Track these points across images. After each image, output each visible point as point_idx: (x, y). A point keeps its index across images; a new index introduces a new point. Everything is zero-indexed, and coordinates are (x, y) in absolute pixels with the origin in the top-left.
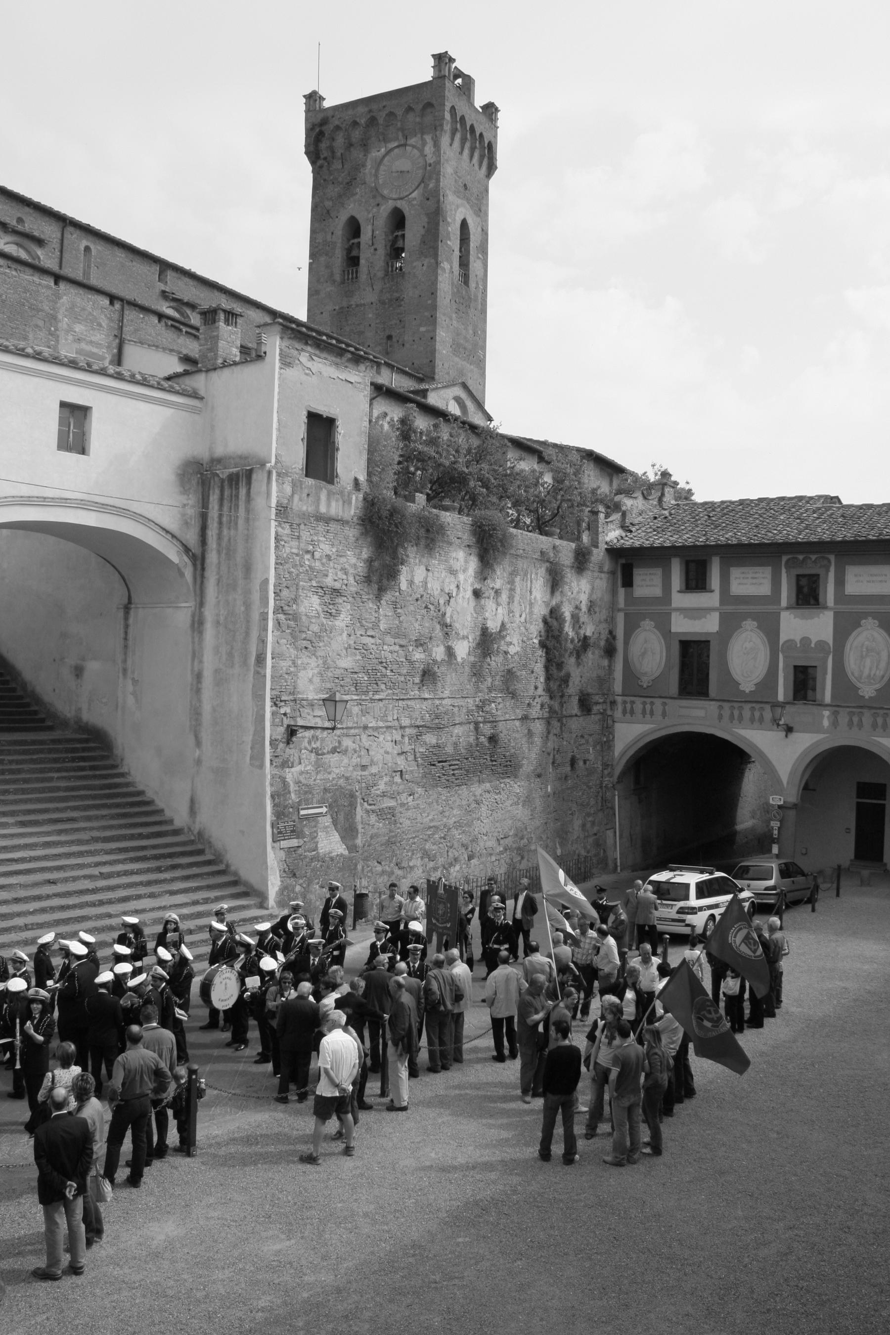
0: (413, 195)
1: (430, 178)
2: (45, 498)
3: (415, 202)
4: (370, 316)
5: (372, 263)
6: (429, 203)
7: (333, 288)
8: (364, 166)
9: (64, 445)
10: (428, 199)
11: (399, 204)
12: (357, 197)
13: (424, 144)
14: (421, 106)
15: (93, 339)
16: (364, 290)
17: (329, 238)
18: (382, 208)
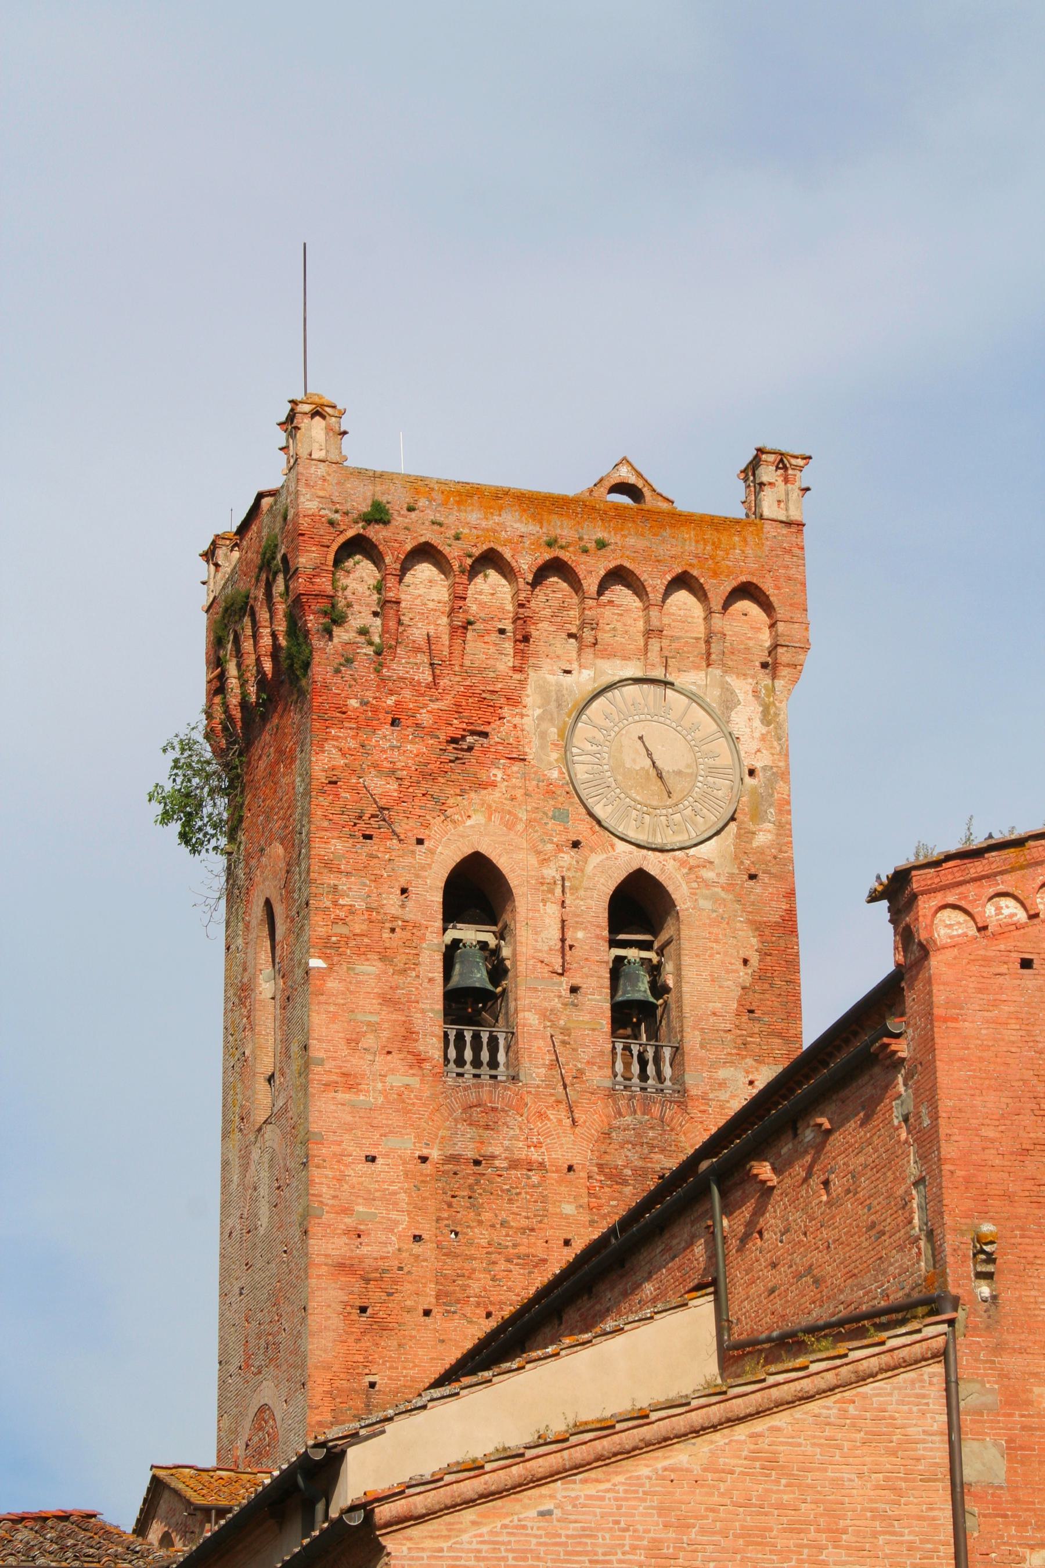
0: (705, 850)
1: (757, 815)
2: (605, 1428)
3: (709, 874)
4: (569, 1209)
5: (566, 1031)
6: (757, 887)
7: (415, 1082)
8: (514, 701)
9: (367, 1157)
10: (752, 877)
11: (654, 865)
12: (494, 796)
13: (729, 702)
14: (728, 586)
15: (251, 649)
16: (541, 1116)
17: (392, 902)
18: (595, 860)
